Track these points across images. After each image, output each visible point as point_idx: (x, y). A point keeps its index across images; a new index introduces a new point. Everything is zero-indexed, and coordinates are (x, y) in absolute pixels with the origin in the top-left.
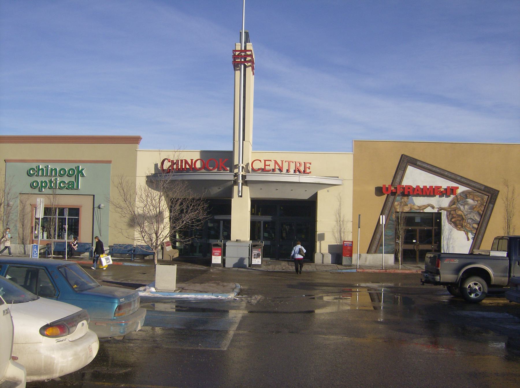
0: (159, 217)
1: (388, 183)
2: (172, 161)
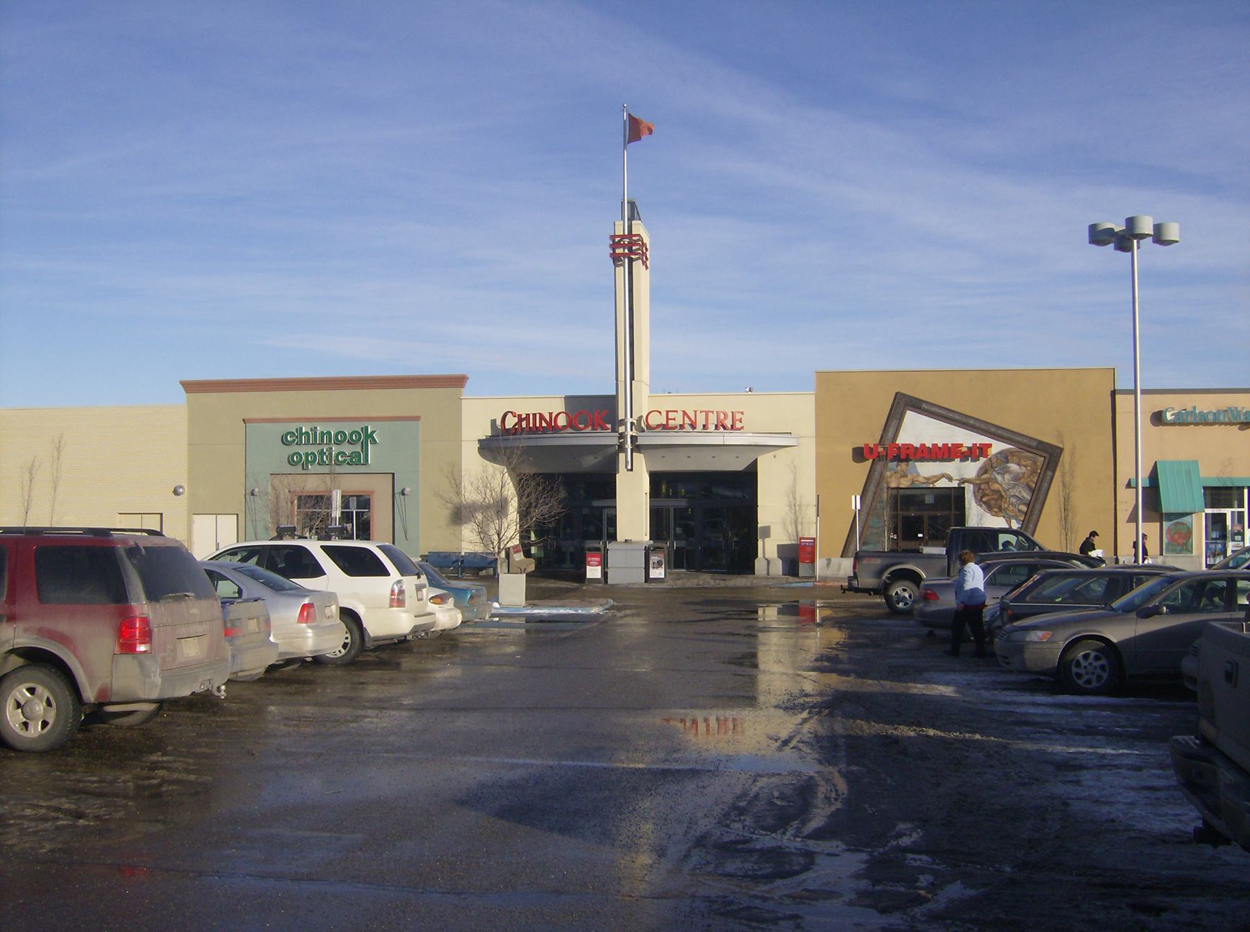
0: (500, 508)
1: (872, 440)
2: (520, 416)
